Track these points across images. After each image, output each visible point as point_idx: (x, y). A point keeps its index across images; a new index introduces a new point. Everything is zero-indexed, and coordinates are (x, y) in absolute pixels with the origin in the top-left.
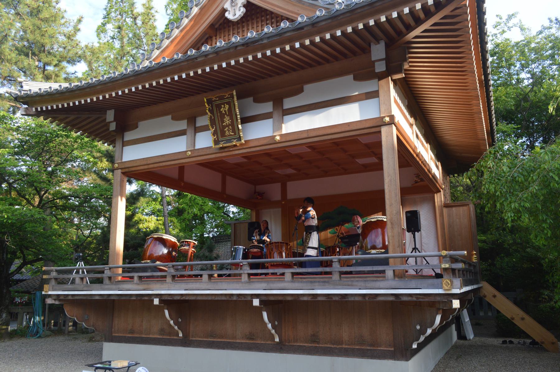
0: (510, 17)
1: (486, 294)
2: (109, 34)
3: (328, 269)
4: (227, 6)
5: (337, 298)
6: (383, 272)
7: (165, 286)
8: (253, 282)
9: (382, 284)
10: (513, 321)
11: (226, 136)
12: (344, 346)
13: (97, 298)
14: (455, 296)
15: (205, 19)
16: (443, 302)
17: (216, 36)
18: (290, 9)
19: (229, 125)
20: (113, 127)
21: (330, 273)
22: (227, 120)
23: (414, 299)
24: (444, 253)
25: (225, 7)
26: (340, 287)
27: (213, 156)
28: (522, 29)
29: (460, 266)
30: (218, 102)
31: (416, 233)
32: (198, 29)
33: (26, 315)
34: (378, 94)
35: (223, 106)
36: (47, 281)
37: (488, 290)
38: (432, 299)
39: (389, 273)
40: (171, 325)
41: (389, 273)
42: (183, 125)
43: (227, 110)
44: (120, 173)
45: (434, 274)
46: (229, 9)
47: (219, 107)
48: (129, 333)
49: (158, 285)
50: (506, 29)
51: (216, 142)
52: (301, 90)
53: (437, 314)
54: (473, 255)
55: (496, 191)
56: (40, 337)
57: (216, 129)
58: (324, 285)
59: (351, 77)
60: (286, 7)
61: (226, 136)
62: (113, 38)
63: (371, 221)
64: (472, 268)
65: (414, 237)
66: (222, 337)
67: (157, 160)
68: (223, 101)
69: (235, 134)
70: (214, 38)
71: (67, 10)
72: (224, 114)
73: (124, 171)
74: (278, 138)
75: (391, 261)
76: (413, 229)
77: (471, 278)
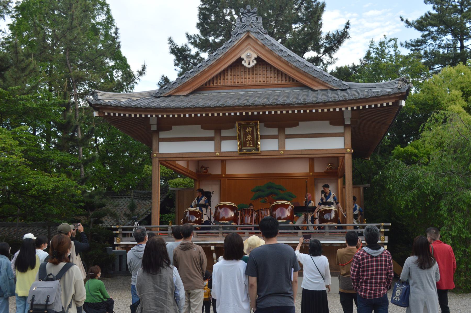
3: (323, 231)
5: (327, 245)
7: (218, 239)
11: (247, 147)
19: (250, 140)
22: (249, 137)
25: (242, 57)
26: (329, 240)
29: (388, 230)
30: (246, 126)
35: (248, 128)
36: (116, 235)
42: (211, 133)
43: (250, 131)
46: (245, 59)
47: (245, 128)
49: (213, 239)
51: (240, 150)
52: (297, 125)
57: (241, 141)
61: (247, 147)
63: (278, 204)
67: (192, 156)
68: (248, 125)
72: (248, 133)
74: (282, 152)
75: (348, 227)
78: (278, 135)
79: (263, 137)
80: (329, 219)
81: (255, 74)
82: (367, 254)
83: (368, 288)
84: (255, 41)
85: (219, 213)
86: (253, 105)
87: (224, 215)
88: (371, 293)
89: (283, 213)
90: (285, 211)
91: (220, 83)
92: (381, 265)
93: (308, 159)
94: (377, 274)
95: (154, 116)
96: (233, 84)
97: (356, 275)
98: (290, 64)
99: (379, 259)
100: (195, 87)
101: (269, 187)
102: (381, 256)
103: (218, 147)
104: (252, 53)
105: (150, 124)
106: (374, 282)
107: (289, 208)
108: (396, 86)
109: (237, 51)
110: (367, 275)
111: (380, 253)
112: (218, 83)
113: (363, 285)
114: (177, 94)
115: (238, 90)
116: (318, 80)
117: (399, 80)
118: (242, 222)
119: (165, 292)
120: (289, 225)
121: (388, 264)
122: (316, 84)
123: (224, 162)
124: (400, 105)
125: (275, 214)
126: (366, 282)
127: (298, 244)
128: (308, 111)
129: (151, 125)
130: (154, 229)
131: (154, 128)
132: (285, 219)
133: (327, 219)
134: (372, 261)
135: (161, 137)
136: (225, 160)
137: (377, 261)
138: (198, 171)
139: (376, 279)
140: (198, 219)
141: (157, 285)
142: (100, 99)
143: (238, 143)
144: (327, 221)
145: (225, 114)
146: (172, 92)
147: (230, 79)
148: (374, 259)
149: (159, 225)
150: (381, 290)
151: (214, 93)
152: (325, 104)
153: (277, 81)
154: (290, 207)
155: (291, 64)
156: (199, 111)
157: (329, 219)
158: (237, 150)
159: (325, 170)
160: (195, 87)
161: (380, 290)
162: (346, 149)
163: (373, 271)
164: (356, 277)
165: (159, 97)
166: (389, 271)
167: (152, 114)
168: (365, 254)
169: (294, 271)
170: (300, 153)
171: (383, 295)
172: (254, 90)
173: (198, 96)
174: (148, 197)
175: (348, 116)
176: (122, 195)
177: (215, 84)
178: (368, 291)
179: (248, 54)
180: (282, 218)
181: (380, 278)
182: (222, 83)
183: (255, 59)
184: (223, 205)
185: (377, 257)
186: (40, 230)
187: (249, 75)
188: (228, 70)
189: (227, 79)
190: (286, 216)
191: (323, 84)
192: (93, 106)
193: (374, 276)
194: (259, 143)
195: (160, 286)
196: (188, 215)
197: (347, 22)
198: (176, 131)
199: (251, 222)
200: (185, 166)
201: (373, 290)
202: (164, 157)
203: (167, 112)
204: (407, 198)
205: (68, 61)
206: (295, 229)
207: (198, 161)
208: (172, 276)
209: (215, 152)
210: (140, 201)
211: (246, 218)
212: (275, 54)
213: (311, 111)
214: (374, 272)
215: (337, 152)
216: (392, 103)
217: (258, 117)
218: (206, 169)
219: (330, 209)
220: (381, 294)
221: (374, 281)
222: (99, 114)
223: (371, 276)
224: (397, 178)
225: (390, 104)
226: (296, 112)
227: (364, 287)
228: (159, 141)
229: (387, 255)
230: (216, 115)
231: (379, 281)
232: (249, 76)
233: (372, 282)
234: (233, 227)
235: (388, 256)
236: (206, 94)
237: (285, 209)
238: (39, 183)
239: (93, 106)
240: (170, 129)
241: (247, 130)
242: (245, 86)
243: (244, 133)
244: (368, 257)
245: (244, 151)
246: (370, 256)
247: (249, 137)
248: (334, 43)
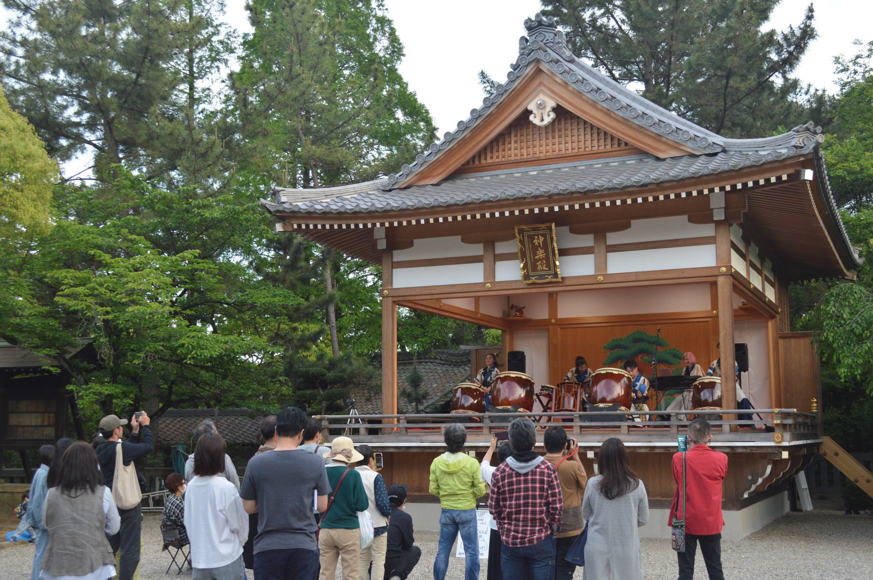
1: (827, 451)
3: (666, 423)
4: (531, 107)
6: (720, 426)
7: (481, 437)
8: (585, 434)
9: (719, 437)
10: (858, 484)
11: (538, 271)
14: (785, 448)
15: (501, 119)
16: (774, 453)
19: (543, 259)
21: (668, 426)
22: (541, 254)
23: (748, 451)
24: (777, 410)
25: (529, 108)
29: (790, 421)
30: (532, 233)
32: (493, 130)
33: (160, 480)
34: (716, 240)
35: (536, 237)
37: (829, 446)
38: (764, 451)
39: (726, 428)
41: (726, 428)
42: (477, 250)
44: (391, 302)
45: (764, 427)
46: (535, 111)
47: (531, 238)
48: (416, 491)
51: (526, 277)
52: (628, 226)
53: (769, 464)
54: (812, 403)
55: (833, 342)
57: (526, 261)
58: (662, 437)
59: (685, 217)
64: (809, 421)
68: (537, 232)
69: (550, 269)
72: (537, 247)
74: (601, 278)
75: (725, 416)
77: (806, 432)
78: (594, 247)
79: (563, 252)
80: (710, 400)
81: (557, 137)
82: (511, 469)
83: (513, 528)
84: (551, 77)
85: (499, 390)
86: (529, 196)
87: (507, 395)
88: (517, 538)
89: (610, 390)
90: (614, 386)
91: (498, 157)
92: (534, 489)
93: (708, 285)
94: (526, 505)
95: (717, 190)
96: (519, 157)
97: (495, 505)
98: (613, 115)
99: (530, 477)
100: (451, 168)
101: (636, 341)
102: (533, 473)
103: (490, 273)
104: (546, 99)
105: (711, 207)
106: (521, 519)
107: (622, 382)
108: (793, 142)
109: (521, 99)
110: (510, 507)
111: (533, 468)
112: (494, 157)
113: (505, 523)
114: (422, 183)
115: (528, 169)
116: (664, 139)
117: (798, 131)
118: (559, 408)
119: (89, 525)
120: (618, 412)
121: (546, 486)
123: (555, 295)
124: (802, 179)
125: (596, 391)
126: (510, 519)
127: (488, 447)
128: (629, 201)
129: (377, 240)
130: (386, 420)
131: (382, 245)
132: (613, 401)
133: (706, 400)
134: (518, 482)
135: (395, 259)
136: (557, 293)
137: (526, 482)
138: (507, 314)
139: (526, 512)
140: (476, 402)
141: (78, 514)
142: (284, 203)
143: (522, 265)
144: (706, 403)
145: (604, 203)
146: (411, 181)
147: (514, 149)
148: (522, 478)
149: (396, 414)
150: (535, 533)
151: (486, 177)
152: (660, 185)
153: (597, 146)
154: (625, 379)
155: (614, 113)
156: (508, 206)
157: (710, 400)
158: (520, 278)
159: (741, 305)
160: (451, 168)
161: (533, 532)
162: (719, 267)
163: (519, 500)
164: (495, 509)
165: (390, 190)
166: (550, 499)
167: (711, 186)
168: (507, 469)
169: (318, 495)
170: (634, 278)
171: (537, 541)
172: (570, 164)
173: (648, 162)
174: (463, 362)
175: (717, 202)
176: (421, 359)
177: (489, 161)
178: (512, 533)
179: (539, 102)
180: (608, 399)
181: (532, 511)
182: (500, 157)
183: (554, 110)
184: (505, 377)
185: (526, 475)
186: (249, 425)
187: (553, 138)
188: (510, 133)
189: (510, 149)
190: (615, 395)
191: (676, 146)
192: (273, 213)
193: (522, 508)
194: (557, 263)
195: (82, 516)
196: (459, 394)
197: (810, 8)
198: (422, 248)
199: (574, 406)
200: (472, 309)
201: (520, 531)
202: (400, 294)
203: (663, 189)
204: (850, 360)
205: (301, 132)
206: (716, 420)
207: (508, 297)
208: (102, 502)
209: (485, 283)
210: (450, 369)
211: (566, 399)
212: (586, 99)
213: (634, 201)
214: (522, 502)
215: (703, 274)
216: (788, 176)
217: (552, 217)
218: (520, 310)
219: (712, 380)
220: (533, 539)
221: (522, 516)
222: (283, 227)
223: (515, 508)
224: (844, 320)
225: (785, 177)
226: (608, 204)
227: (506, 526)
228: (393, 268)
229: (546, 471)
230: (598, 205)
231: (529, 516)
232: (516, 145)
233: (519, 518)
234: (624, 415)
235: (548, 473)
236: (460, 183)
237: (614, 383)
238: (200, 347)
239: (273, 213)
240: (410, 245)
241: (536, 241)
242: (539, 160)
243: (531, 246)
244: (512, 474)
245: (533, 280)
246: (514, 473)
247: (541, 254)
248: (787, 51)
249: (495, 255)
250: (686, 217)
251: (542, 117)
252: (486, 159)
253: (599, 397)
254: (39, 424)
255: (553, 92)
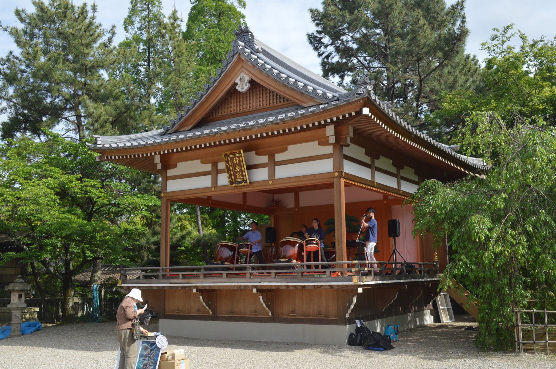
0: (506, 29)
2: (136, 26)
4: (237, 81)
7: (200, 280)
11: (237, 179)
12: (310, 318)
13: (155, 288)
17: (231, 98)
18: (280, 89)
20: (159, 167)
25: (236, 81)
27: (230, 191)
28: (522, 37)
30: (232, 156)
31: (396, 238)
32: (217, 96)
40: (204, 306)
44: (165, 200)
46: (239, 83)
47: (232, 159)
49: (236, 280)
50: (505, 39)
51: (231, 183)
53: (354, 296)
54: (435, 256)
56: (99, 322)
59: (316, 143)
60: (277, 87)
62: (140, 29)
65: (395, 241)
66: (238, 314)
70: (230, 99)
71: (102, 24)
73: (168, 198)
75: (337, 266)
76: (393, 235)
95: (157, 153)
105: (327, 135)
122: (305, 100)
125: (281, 251)
147: (233, 107)
149: (168, 267)
183: (250, 82)
198: (182, 167)
228: (275, 166)
241: (234, 161)
249: (275, 162)
250: (317, 142)
251: (243, 87)
252: (219, 114)
253: (283, 255)
254: (13, 274)
255: (249, 71)
